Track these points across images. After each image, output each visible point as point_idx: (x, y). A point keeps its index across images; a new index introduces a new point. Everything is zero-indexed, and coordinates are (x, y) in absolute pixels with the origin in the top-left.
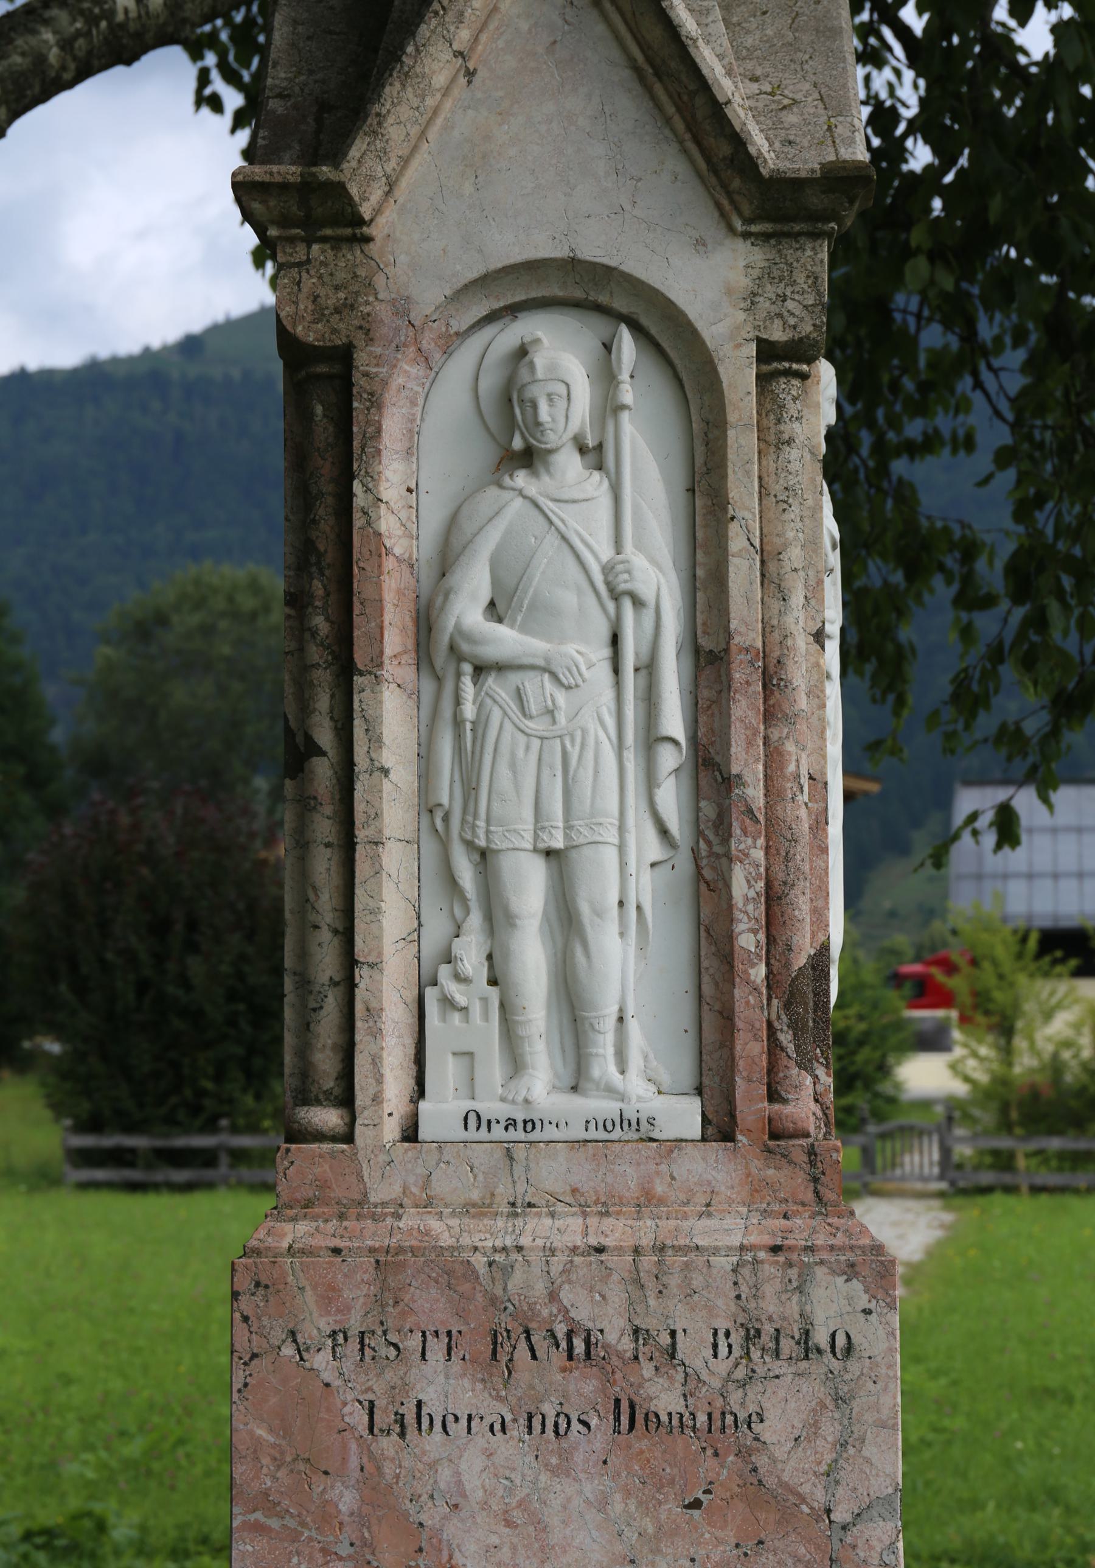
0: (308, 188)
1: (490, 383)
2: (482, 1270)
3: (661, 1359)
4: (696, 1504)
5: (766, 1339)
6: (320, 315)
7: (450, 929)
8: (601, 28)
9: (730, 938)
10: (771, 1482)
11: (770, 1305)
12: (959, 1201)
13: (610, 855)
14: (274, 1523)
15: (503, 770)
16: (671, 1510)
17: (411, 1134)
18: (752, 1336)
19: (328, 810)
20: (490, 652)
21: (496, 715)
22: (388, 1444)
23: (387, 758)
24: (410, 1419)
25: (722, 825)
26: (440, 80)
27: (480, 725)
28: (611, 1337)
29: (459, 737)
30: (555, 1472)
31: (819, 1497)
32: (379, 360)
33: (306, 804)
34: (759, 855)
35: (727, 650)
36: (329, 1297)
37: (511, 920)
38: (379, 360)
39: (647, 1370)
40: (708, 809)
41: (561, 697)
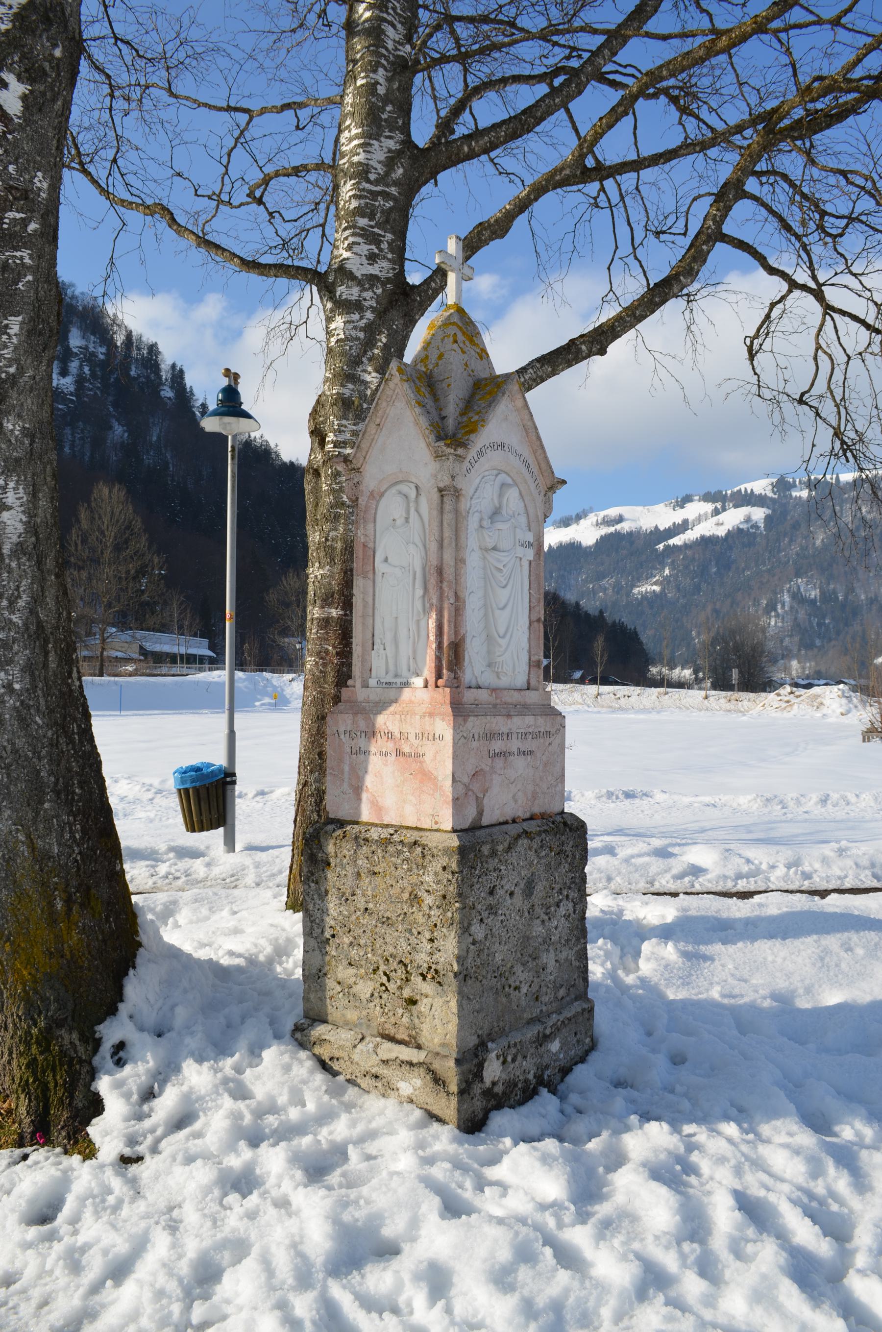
22: (354, 756)
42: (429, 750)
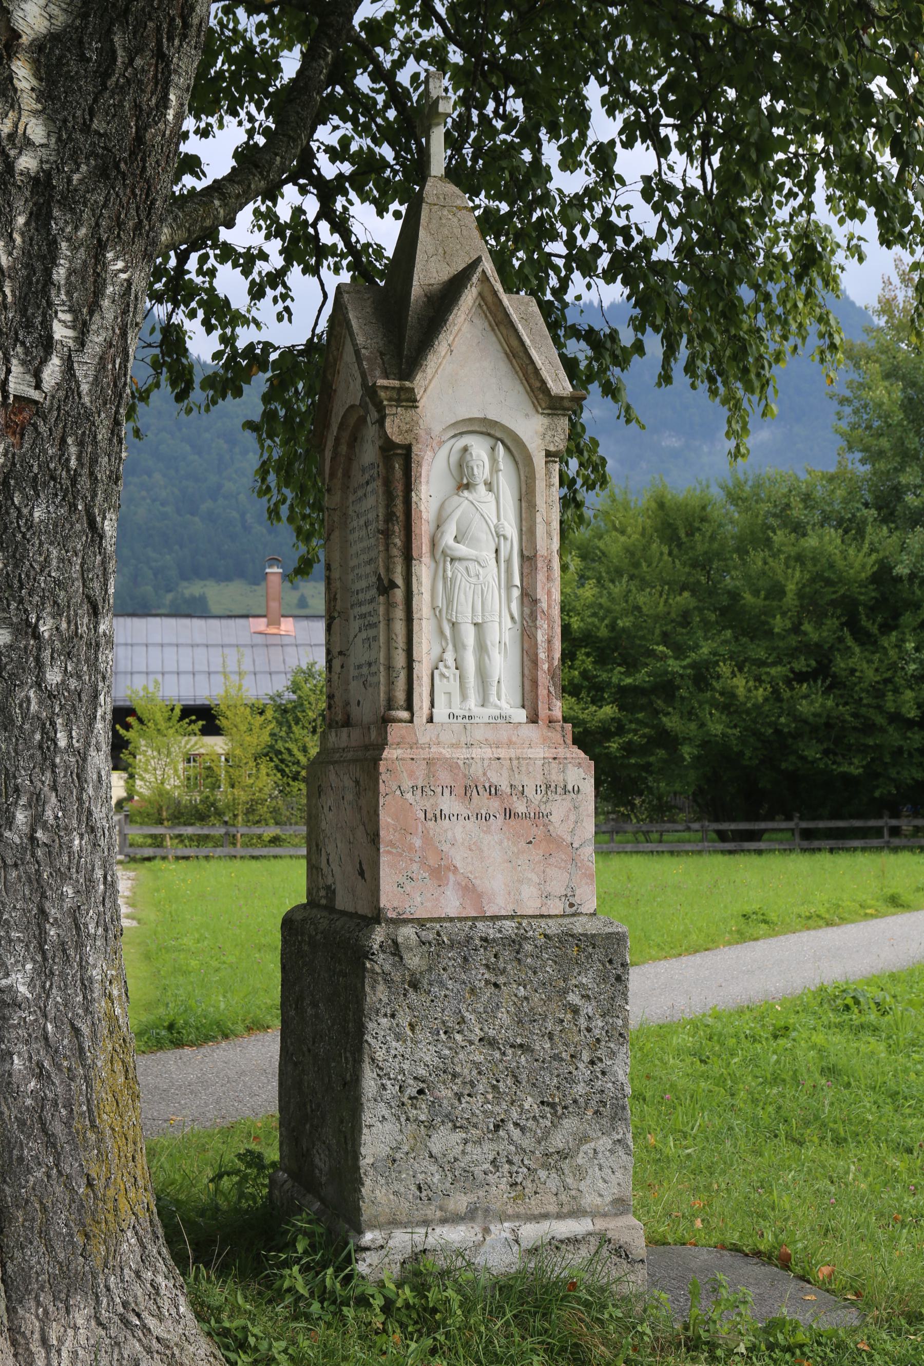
0: (401, 389)
1: (454, 459)
2: (462, 765)
3: (519, 795)
4: (530, 842)
5: (553, 788)
6: (400, 433)
7: (441, 650)
8: (494, 339)
9: (536, 655)
10: (554, 835)
11: (554, 777)
12: (133, 865)
13: (497, 625)
14: (394, 851)
15: (462, 596)
16: (523, 844)
17: (430, 720)
18: (548, 787)
19: (401, 607)
20: (457, 554)
21: (459, 575)
22: (431, 824)
23: (423, 590)
24: (438, 816)
25: (533, 616)
26: (443, 354)
27: (453, 579)
28: (503, 788)
29: (445, 583)
30: (485, 832)
31: (569, 840)
32: (421, 450)
33: (390, 605)
34: (546, 626)
35: (535, 556)
36: (411, 774)
37: (464, 647)
38: (421, 450)
39: (515, 798)
40: (527, 611)
41: (481, 570)
42: (558, 809)
